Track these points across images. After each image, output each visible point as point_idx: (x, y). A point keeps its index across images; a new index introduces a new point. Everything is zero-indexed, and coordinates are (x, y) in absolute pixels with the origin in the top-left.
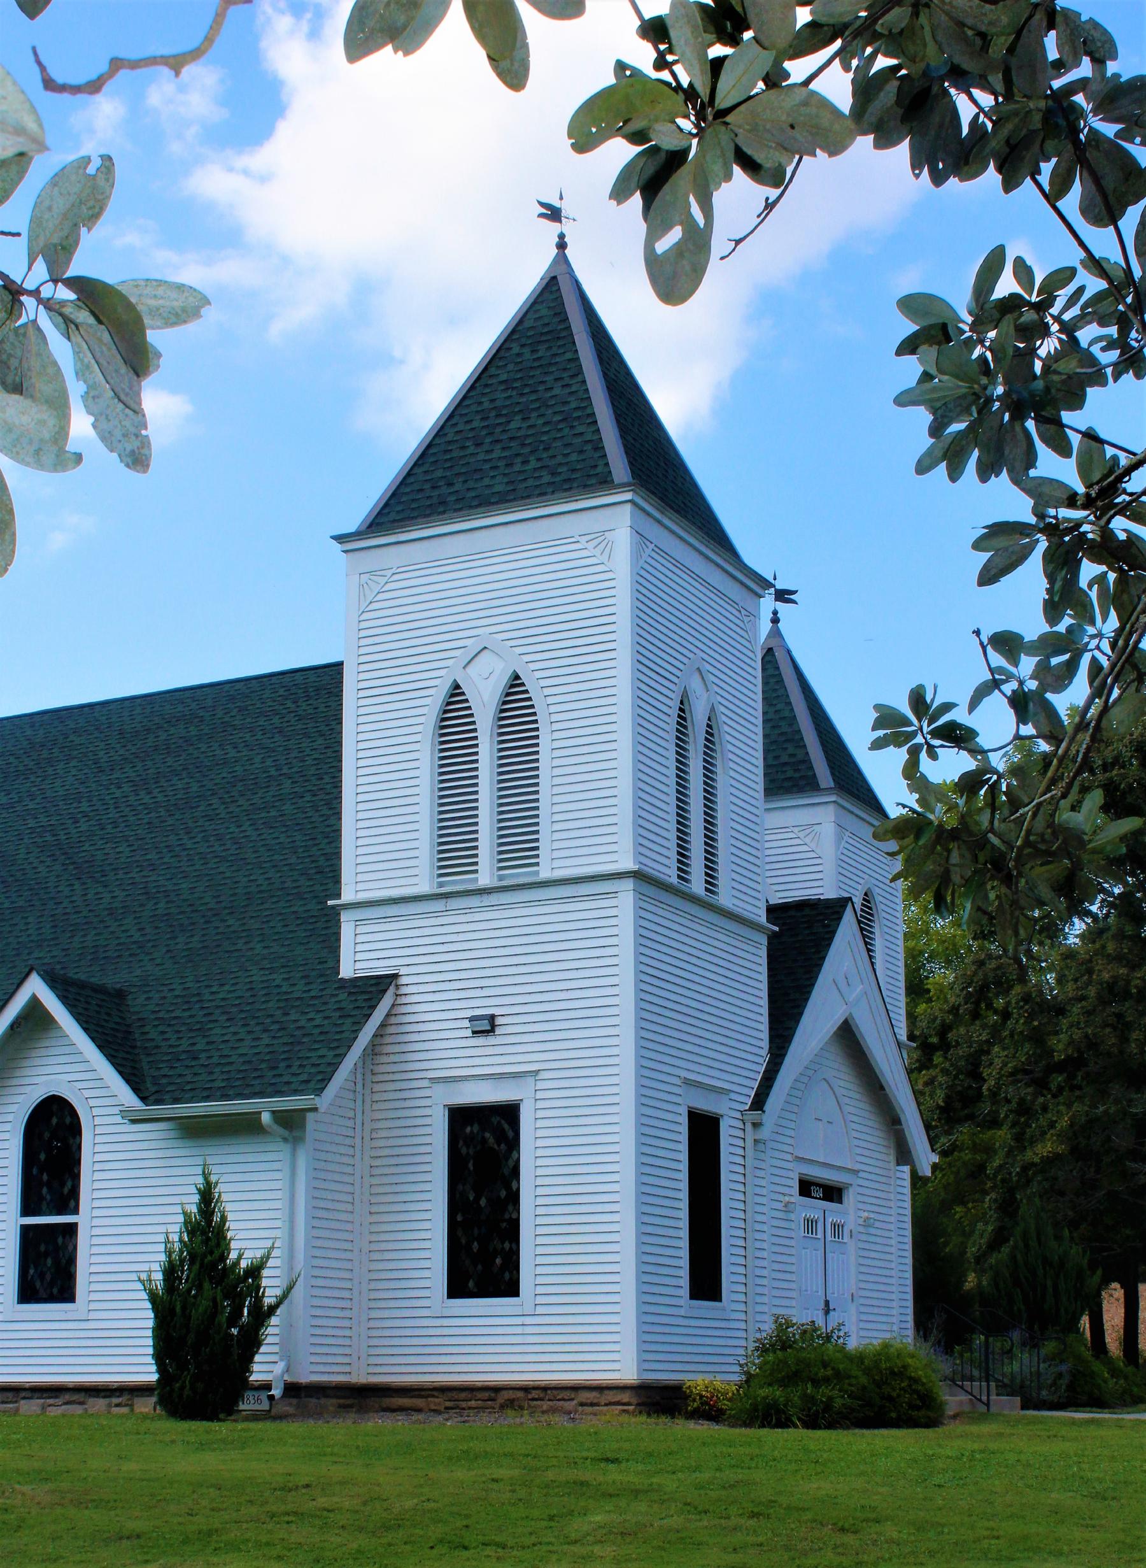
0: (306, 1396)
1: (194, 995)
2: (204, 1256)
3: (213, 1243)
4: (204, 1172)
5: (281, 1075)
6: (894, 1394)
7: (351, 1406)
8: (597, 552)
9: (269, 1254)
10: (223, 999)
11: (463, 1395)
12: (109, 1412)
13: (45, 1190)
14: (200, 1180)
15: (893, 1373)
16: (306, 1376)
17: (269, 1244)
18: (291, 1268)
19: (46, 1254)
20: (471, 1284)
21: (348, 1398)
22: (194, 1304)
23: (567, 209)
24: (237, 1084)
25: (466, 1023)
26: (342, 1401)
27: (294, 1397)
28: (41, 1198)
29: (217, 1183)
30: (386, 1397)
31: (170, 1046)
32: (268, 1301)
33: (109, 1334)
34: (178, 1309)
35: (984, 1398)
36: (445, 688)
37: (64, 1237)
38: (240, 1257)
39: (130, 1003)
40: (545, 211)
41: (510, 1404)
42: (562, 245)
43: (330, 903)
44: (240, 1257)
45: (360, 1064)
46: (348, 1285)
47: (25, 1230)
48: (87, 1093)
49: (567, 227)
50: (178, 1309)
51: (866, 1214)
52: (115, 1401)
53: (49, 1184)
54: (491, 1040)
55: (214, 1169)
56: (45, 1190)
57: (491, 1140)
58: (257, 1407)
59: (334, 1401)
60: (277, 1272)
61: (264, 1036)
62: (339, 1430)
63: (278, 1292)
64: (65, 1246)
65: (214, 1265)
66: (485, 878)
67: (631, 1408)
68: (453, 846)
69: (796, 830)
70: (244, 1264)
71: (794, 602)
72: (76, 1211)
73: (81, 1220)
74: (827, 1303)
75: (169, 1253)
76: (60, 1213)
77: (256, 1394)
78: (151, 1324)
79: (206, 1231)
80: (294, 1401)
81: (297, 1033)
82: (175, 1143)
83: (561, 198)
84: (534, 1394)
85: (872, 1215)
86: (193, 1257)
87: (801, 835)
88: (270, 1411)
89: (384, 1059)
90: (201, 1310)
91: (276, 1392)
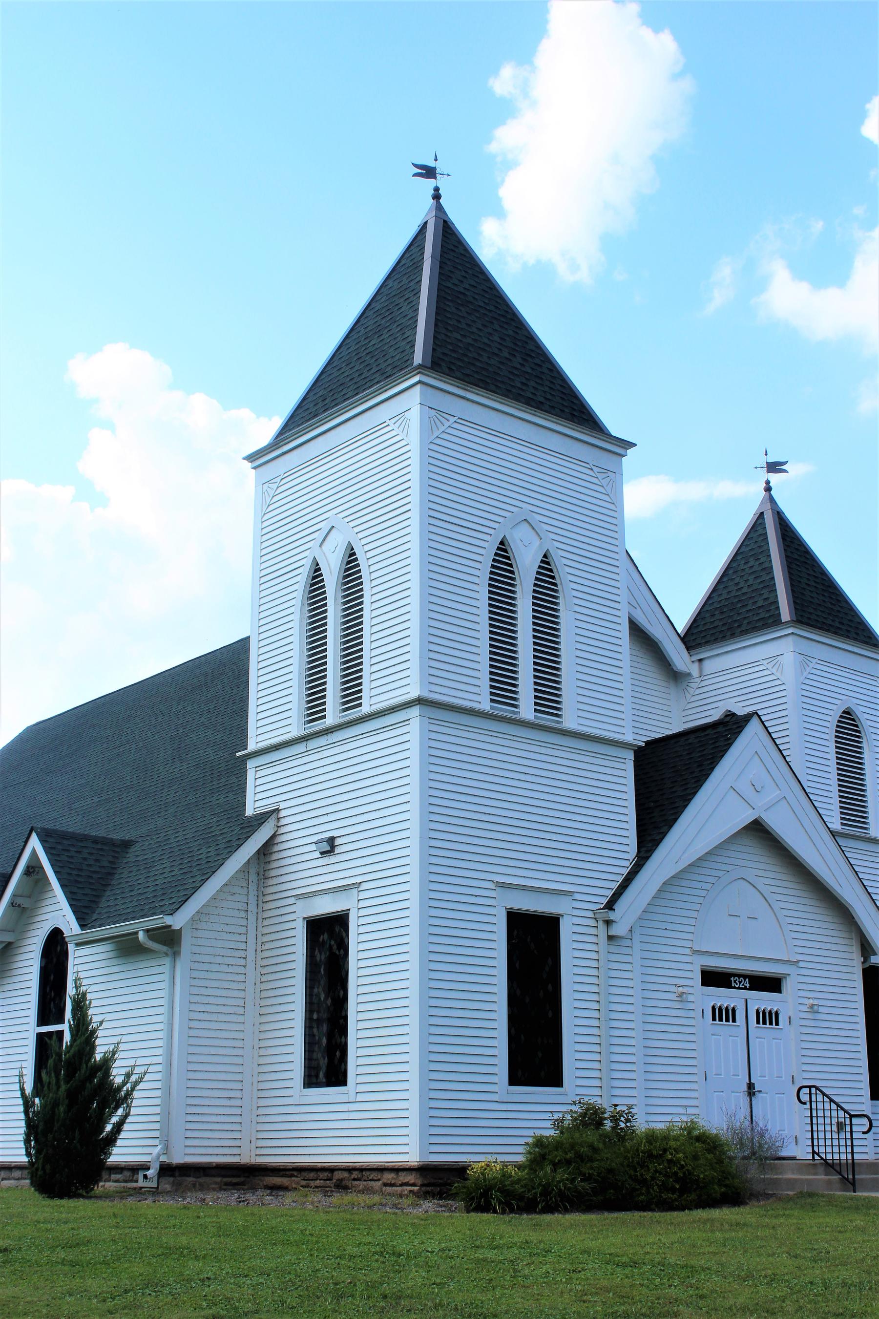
0: (180, 1176)
11: (312, 1175)
15: (651, 1156)
16: (178, 1158)
21: (239, 1176)
23: (440, 167)
30: (267, 1176)
35: (851, 1177)
36: (308, 563)
40: (420, 171)
41: (341, 1186)
42: (437, 196)
43: (238, 754)
49: (441, 182)
51: (811, 1001)
57: (335, 947)
59: (219, 1179)
62: (221, 1207)
66: (331, 718)
67: (416, 1188)
69: (765, 662)
71: (785, 471)
74: (751, 1086)
82: (115, 961)
83: (436, 160)
84: (355, 1174)
85: (816, 1002)
88: (157, 1188)
89: (271, 882)
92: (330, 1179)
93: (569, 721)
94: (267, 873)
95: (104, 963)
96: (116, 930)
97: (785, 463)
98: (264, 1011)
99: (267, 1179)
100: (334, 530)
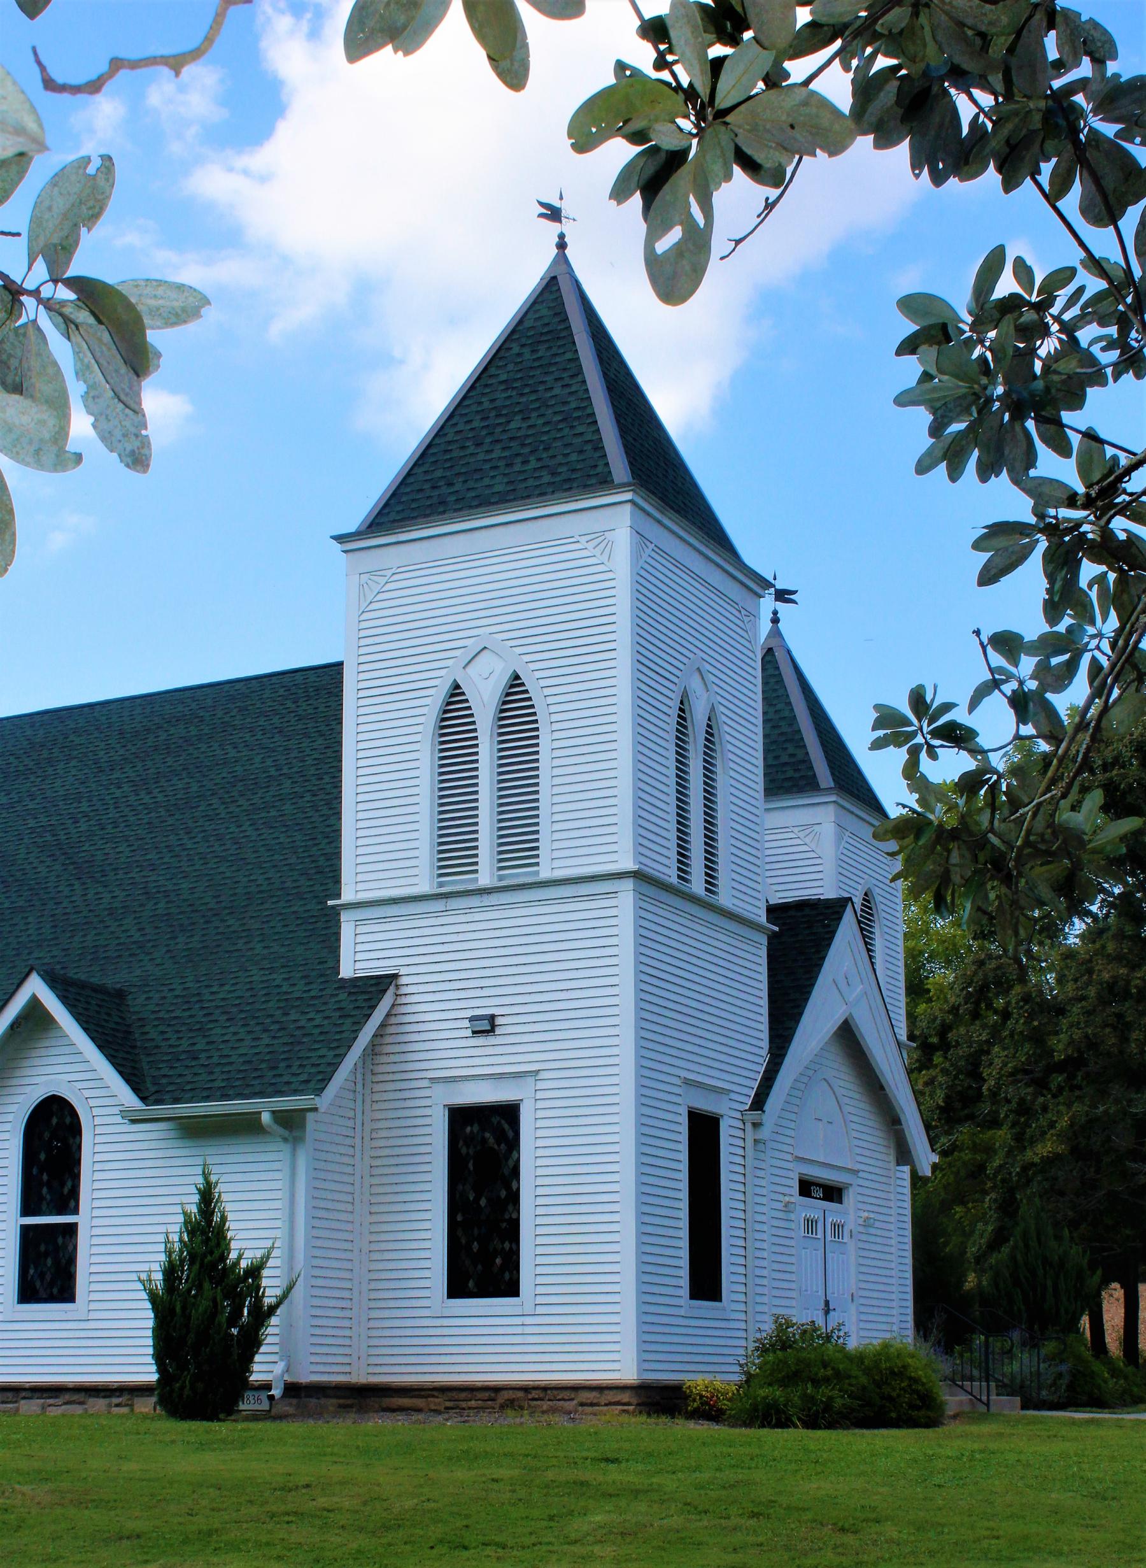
0: (306, 1396)
1: (194, 995)
2: (204, 1255)
3: (213, 1243)
4: (204, 1172)
5: (281, 1075)
6: (894, 1394)
7: (351, 1406)
8: (597, 552)
9: (269, 1254)
10: (223, 999)
11: (463, 1395)
12: (109, 1412)
13: (45, 1190)
14: (200, 1180)
15: (893, 1373)
16: (306, 1376)
17: (269, 1244)
18: (291, 1268)
19: (46, 1254)
20: (471, 1284)
22: (194, 1305)
24: (237, 1083)
25: (466, 1023)
26: (342, 1401)
27: (294, 1397)
28: (41, 1198)
29: (217, 1183)
30: (386, 1397)
31: (170, 1046)
32: (267, 1301)
33: (109, 1334)
34: (178, 1309)
35: (984, 1398)
37: (64, 1237)
38: (240, 1257)
39: (130, 1003)
40: (545, 211)
42: (562, 245)
44: (240, 1257)
45: (360, 1065)
46: (348, 1285)
47: (25, 1230)
48: (87, 1093)
49: (567, 227)
50: (178, 1309)
51: (866, 1214)
52: (115, 1401)
53: (49, 1184)
54: (491, 1040)
55: (215, 1169)
56: (45, 1190)
58: (257, 1407)
59: (334, 1401)
60: (277, 1272)
61: (264, 1036)
62: (339, 1430)
63: (278, 1292)
64: (65, 1246)
65: (214, 1266)
66: (485, 878)
67: (631, 1408)
68: (453, 845)
70: (244, 1264)
72: (76, 1211)
73: (81, 1220)
74: (827, 1303)
75: (169, 1253)
76: (60, 1213)
77: (256, 1394)
78: (151, 1324)
79: (206, 1231)
80: (294, 1401)
81: (297, 1033)
82: (176, 1143)
83: (561, 198)
84: (534, 1394)
85: (872, 1215)
86: (193, 1257)
87: (801, 835)
88: (270, 1411)
89: (384, 1059)
90: (201, 1309)
91: (276, 1392)
92: (493, 1400)
93: (725, 899)
94: (377, 1049)
95: (153, 1145)
96: (220, 1108)
97: (794, 592)
98: (375, 1209)
99: (388, 1400)
100: (486, 651)
